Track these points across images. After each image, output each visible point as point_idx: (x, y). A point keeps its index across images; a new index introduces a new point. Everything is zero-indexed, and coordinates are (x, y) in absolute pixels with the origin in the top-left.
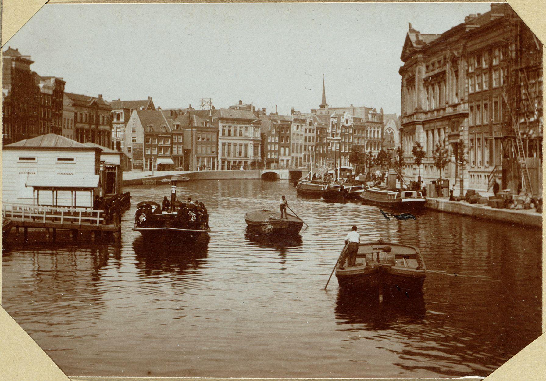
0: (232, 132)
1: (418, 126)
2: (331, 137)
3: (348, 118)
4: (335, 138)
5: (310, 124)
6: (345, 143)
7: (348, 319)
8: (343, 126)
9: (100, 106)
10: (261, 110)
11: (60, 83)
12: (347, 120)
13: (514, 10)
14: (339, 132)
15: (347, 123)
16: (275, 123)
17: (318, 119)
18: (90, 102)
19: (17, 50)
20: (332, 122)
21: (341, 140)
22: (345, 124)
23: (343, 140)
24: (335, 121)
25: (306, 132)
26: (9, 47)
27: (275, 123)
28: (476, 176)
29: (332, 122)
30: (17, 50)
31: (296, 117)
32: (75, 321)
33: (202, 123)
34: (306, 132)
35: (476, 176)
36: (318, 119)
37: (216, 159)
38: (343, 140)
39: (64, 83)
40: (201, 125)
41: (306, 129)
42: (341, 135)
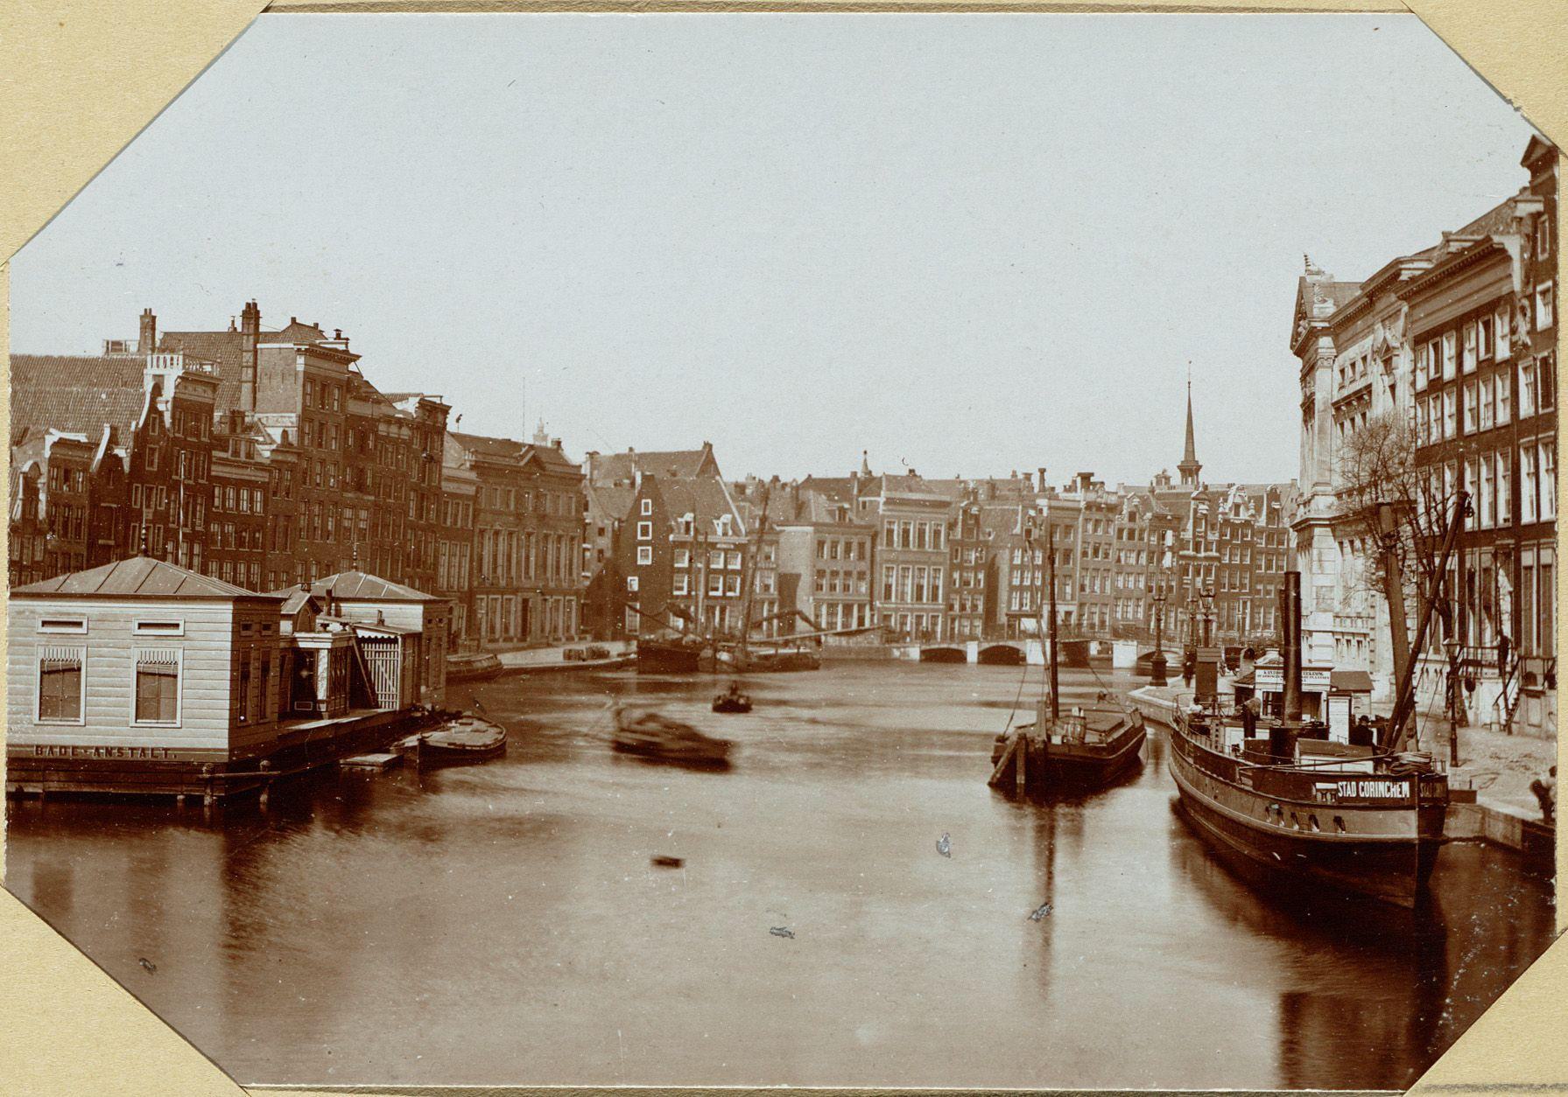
0: (840, 549)
1: (1317, 531)
2: (1191, 553)
3: (1238, 500)
4: (1203, 554)
5: (1132, 517)
6: (1230, 566)
7: (173, 423)
8: (1227, 521)
9: (408, 700)
10: (1020, 476)
11: (434, 411)
12: (1237, 506)
13: (831, 475)
14: (1213, 537)
15: (1237, 514)
16: (1032, 513)
17: (1154, 502)
18: (522, 457)
19: (316, 325)
20: (1196, 511)
21: (1219, 559)
22: (1232, 516)
23: (1226, 560)
24: (1203, 508)
25: (1120, 537)
26: (294, 320)
27: (1032, 513)
28: (1354, 642)
29: (1196, 511)
30: (316, 325)
31: (1092, 496)
32: (471, 561)
33: (831, 513)
34: (1120, 537)
35: (1354, 642)
36: (1154, 502)
37: (868, 608)
38: (1226, 560)
39: (445, 410)
40: (828, 520)
41: (1120, 531)
42: (1221, 545)
